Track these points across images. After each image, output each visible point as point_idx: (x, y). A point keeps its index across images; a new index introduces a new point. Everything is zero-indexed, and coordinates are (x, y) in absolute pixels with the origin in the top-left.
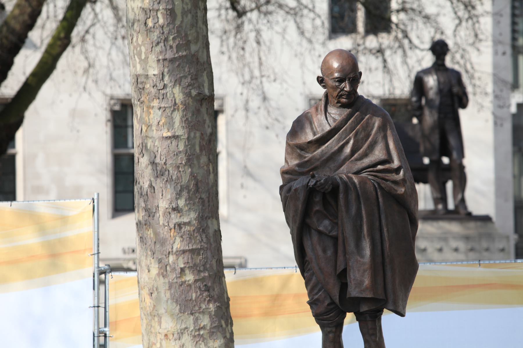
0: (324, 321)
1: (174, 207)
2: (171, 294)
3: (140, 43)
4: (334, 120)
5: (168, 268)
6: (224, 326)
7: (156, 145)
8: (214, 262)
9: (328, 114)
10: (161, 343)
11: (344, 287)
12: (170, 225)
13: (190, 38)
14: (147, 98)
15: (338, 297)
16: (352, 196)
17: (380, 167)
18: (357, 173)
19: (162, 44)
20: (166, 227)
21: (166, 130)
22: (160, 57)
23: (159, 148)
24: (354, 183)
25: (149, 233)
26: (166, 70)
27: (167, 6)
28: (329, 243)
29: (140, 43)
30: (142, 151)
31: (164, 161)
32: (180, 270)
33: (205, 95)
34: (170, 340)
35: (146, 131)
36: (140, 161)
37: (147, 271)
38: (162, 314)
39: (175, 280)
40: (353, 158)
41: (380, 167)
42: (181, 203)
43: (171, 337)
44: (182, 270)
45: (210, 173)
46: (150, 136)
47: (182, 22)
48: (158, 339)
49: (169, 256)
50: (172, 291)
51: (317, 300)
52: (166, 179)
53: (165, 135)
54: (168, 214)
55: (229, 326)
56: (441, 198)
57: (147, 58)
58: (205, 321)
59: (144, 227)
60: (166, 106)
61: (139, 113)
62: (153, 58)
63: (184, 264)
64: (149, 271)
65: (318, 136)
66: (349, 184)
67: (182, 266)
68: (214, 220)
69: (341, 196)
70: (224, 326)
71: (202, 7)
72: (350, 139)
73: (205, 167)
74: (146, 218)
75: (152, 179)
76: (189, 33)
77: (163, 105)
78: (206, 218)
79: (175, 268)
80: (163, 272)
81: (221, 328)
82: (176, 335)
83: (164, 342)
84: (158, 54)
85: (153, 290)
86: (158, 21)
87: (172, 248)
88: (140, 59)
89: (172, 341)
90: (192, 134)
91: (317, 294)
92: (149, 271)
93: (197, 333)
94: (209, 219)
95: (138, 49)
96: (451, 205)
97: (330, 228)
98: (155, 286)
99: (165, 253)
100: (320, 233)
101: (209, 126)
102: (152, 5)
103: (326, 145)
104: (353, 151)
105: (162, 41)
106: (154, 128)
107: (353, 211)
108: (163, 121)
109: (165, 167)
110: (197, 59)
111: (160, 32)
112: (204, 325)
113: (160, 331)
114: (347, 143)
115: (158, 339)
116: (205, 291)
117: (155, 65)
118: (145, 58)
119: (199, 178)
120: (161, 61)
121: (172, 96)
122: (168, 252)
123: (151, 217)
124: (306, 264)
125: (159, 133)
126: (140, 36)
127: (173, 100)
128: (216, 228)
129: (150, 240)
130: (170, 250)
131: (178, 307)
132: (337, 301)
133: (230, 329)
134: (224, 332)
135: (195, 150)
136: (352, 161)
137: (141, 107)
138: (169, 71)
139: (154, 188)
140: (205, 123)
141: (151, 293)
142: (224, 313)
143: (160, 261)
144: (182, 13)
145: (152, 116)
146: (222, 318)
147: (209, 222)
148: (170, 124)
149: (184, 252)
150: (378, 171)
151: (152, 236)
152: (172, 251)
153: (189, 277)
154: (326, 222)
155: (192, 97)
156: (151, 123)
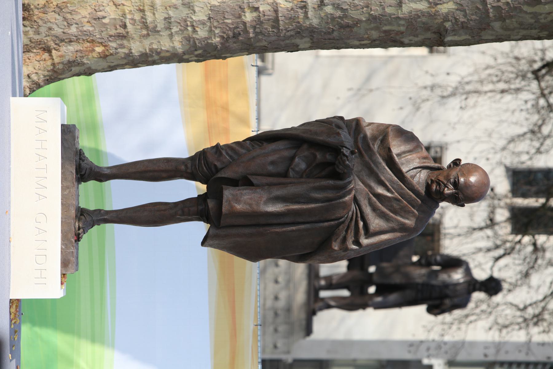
0: (199, 160)
4: (413, 177)
6: (196, 53)
9: (420, 169)
11: (234, 183)
13: (507, 21)
15: (223, 176)
17: (361, 224)
24: (344, 196)
28: (280, 168)
33: (444, 37)
41: (361, 224)
45: (360, 41)
47: (526, 12)
51: (221, 154)
55: (196, 58)
63: (263, 12)
66: (344, 191)
67: (261, 9)
70: (196, 53)
71: (541, 35)
72: (392, 193)
73: (367, 36)
76: (514, 20)
90: (402, 22)
91: (227, 153)
94: (311, 39)
96: (324, 294)
97: (297, 169)
100: (292, 158)
104: (378, 196)
114: (388, 190)
116: (234, 34)
119: (355, 29)
128: (301, 46)
132: (219, 175)
135: (386, 25)
136: (369, 195)
140: (414, 36)
142: (210, 53)
144: (536, 13)
146: (205, 51)
153: (249, 17)
154: (303, 166)
155: (443, 22)
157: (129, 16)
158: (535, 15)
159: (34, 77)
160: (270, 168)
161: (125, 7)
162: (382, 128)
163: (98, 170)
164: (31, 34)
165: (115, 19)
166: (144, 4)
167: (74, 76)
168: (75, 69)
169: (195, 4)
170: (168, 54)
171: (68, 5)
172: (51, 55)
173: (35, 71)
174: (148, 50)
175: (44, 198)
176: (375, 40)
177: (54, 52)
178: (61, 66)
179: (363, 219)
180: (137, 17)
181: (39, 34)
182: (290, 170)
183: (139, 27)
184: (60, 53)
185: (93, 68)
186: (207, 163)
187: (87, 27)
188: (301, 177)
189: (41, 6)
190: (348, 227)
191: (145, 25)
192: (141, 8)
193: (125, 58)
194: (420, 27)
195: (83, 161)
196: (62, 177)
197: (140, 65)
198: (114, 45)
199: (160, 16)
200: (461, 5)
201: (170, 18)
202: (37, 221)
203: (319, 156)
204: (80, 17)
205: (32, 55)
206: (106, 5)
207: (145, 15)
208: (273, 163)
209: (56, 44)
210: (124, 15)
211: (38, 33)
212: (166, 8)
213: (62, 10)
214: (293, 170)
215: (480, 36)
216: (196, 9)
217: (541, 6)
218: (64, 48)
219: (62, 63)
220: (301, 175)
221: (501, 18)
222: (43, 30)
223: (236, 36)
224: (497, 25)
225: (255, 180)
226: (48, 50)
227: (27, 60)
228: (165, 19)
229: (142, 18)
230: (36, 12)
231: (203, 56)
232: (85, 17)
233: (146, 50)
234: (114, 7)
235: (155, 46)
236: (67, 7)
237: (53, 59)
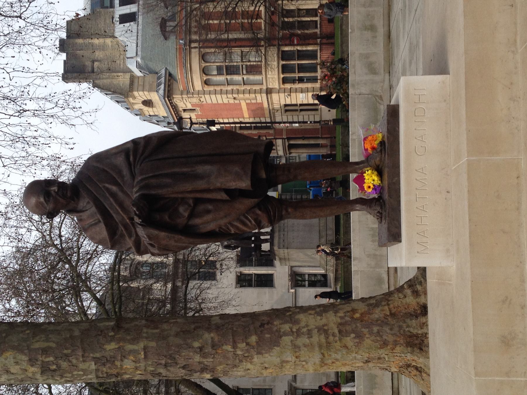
0: (275, 216)
1: (199, 350)
2: (267, 353)
3: (70, 375)
4: (88, 203)
5: (246, 355)
6: (290, 313)
7: (151, 364)
8: (243, 319)
9: (84, 209)
10: (302, 361)
11: (241, 193)
12: (213, 353)
13: (68, 336)
14: (114, 370)
15: (253, 200)
16: (153, 181)
17: (131, 159)
18: (133, 176)
19: (70, 358)
20: (215, 356)
21: (140, 356)
22: (81, 359)
23: (154, 361)
24: (142, 180)
25: (220, 369)
26: (91, 355)
27: (39, 354)
28: (201, 207)
29: (70, 375)
30: (157, 374)
31: (163, 357)
32: (247, 346)
33: (115, 325)
34: (300, 354)
35: (140, 371)
36: (165, 376)
37: (249, 371)
38: (281, 360)
39: (256, 349)
40: (122, 184)
41: (131, 159)
42: (196, 344)
43: (298, 354)
44: (248, 344)
45: (177, 322)
46: (144, 368)
47: (54, 342)
48: (299, 363)
49: (238, 354)
50: (264, 352)
51: (255, 220)
52: (178, 356)
53: (143, 357)
54: (205, 355)
55: (291, 309)
56: (266, 241)
57: (82, 370)
58: (286, 327)
59: (215, 373)
60: (120, 356)
61: (128, 376)
62: (82, 366)
63: (243, 343)
64: (249, 369)
65: (101, 219)
66: (142, 184)
67: (245, 344)
68: (212, 319)
69: (153, 192)
70: (290, 313)
71: (47, 326)
72: (104, 187)
73: (171, 325)
74: (208, 371)
75: (178, 367)
76: (64, 337)
77: (120, 358)
78: (210, 325)
79: (246, 350)
80: (248, 358)
81: (293, 316)
82: (297, 350)
83: (302, 359)
84: (78, 361)
85: (263, 366)
86: (52, 361)
87: (231, 352)
88: (83, 375)
89: (301, 353)
90: (145, 335)
91: (250, 221)
92: (249, 369)
93: (295, 333)
94: (210, 323)
95: (75, 376)
96: (268, 237)
97: (186, 206)
98: (260, 365)
99: (234, 357)
100: (191, 216)
101: (140, 322)
102: (38, 366)
103: (109, 209)
104: (116, 184)
105: (68, 358)
106: (138, 365)
107: (168, 181)
108: (132, 358)
109: (168, 357)
110: (85, 330)
111: (60, 360)
112: (289, 328)
113: (293, 361)
114: (107, 189)
115: (299, 363)
116: (264, 327)
117: (87, 364)
118: (82, 372)
119: (179, 330)
120: (84, 359)
121: (113, 351)
122: (234, 355)
123: (208, 367)
124: (223, 231)
125: (141, 361)
126: (65, 375)
127: (116, 350)
128: (217, 318)
129: (225, 369)
130: (232, 353)
131: (275, 347)
132: (256, 200)
133: (293, 309)
134: (295, 313)
135: (156, 333)
136: (123, 184)
137: (122, 375)
138: (92, 353)
139: (185, 365)
140: (137, 325)
141: (265, 368)
142: (281, 313)
143: (241, 361)
144: (47, 342)
145: (128, 367)
146: (285, 314)
147: (213, 323)
148: (135, 352)
149: (235, 342)
150: (135, 159)
151: (222, 367)
152: (233, 352)
153: (253, 339)
154: (181, 209)
155: (115, 335)
156: (133, 367)
157: (337, 338)
158: (47, 340)
159: (401, 295)
160: (210, 207)
161: (340, 345)
162: (117, 246)
163: (364, 206)
164: (404, 325)
165: (347, 337)
166: (327, 347)
167: (374, 297)
168: (373, 301)
169: (291, 348)
170: (310, 312)
171: (379, 346)
172: (390, 311)
173: (401, 300)
174: (324, 315)
175: (419, 169)
176: (166, 322)
177: (388, 314)
178: (383, 303)
179: (129, 164)
180: (331, 338)
181: (399, 326)
182: (192, 205)
183: (330, 331)
184: (384, 312)
185: (360, 302)
186: (267, 212)
187: (365, 331)
188: (183, 199)
189: (398, 346)
190: (142, 154)
191: (326, 332)
192: (328, 345)
193: (339, 309)
194: (132, 332)
195: (379, 212)
196: (400, 193)
197: (329, 305)
198: (348, 319)
199: (315, 339)
200: (100, 347)
201: (308, 338)
202: (424, 148)
203: (166, 218)
204: (371, 338)
205: (404, 311)
206: (353, 346)
207: (326, 339)
208: (208, 212)
209: (387, 319)
210: (340, 340)
211: (400, 327)
212: (311, 345)
213: (384, 343)
214: (190, 206)
215: (90, 325)
216: (290, 344)
217: (42, 346)
218: (381, 316)
219: (382, 306)
220: (183, 201)
221: (72, 337)
222: (396, 329)
223: (262, 325)
224: (77, 333)
225: (224, 196)
226: (392, 315)
227: (406, 307)
228: (312, 337)
229: (328, 338)
230: (402, 342)
231: (286, 311)
232: (367, 338)
233: (196, 52)
234: (347, 346)
235: (319, 318)
236: (380, 345)
237: (389, 308)
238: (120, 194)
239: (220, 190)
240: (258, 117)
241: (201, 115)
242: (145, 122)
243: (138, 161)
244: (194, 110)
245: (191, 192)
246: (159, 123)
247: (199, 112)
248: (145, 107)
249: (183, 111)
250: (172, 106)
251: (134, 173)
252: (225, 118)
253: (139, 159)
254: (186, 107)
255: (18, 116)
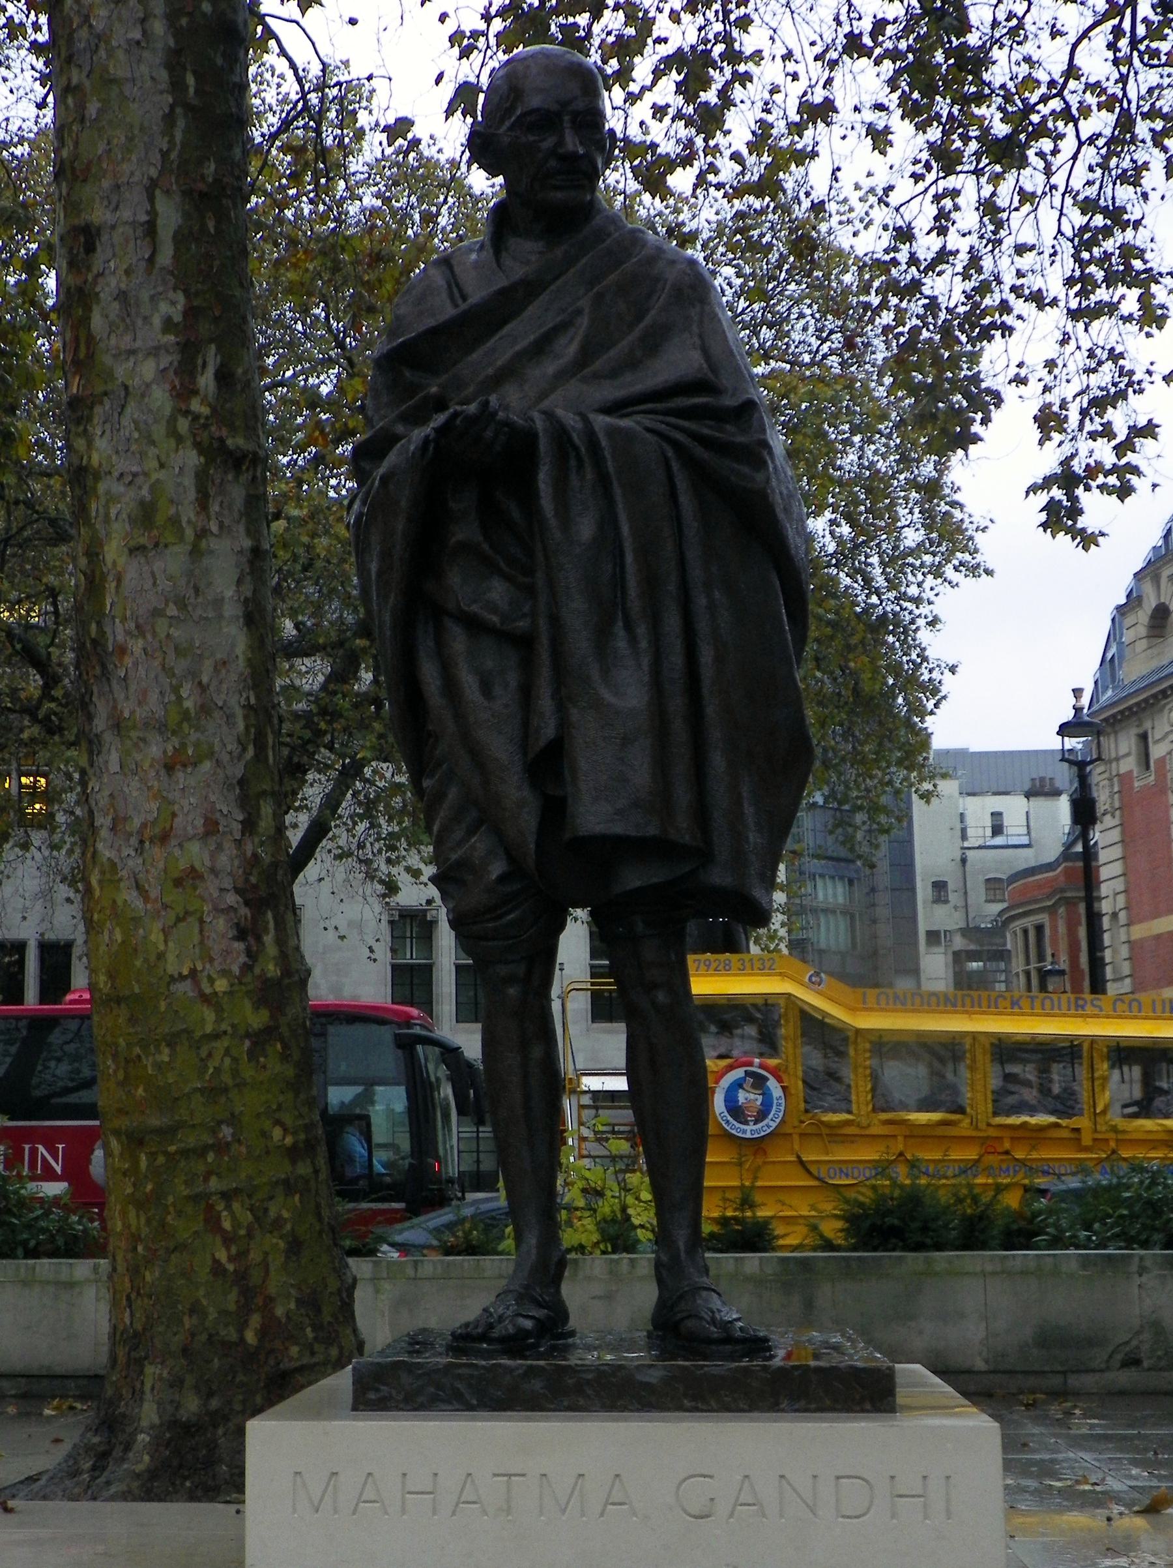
40: (587, 371)
72: (579, 312)
238: (550, 367)
239: (564, 724)
240: (1133, 968)
241: (1132, 788)
242: (1109, 623)
243: (668, 424)
244: (1148, 767)
245: (555, 621)
246: (1107, 665)
247: (1141, 783)
248: (1149, 612)
249: (1141, 731)
250: (1154, 696)
251: (630, 410)
252: (1125, 864)
253: (676, 427)
254: (1157, 742)
255: (1059, 231)
